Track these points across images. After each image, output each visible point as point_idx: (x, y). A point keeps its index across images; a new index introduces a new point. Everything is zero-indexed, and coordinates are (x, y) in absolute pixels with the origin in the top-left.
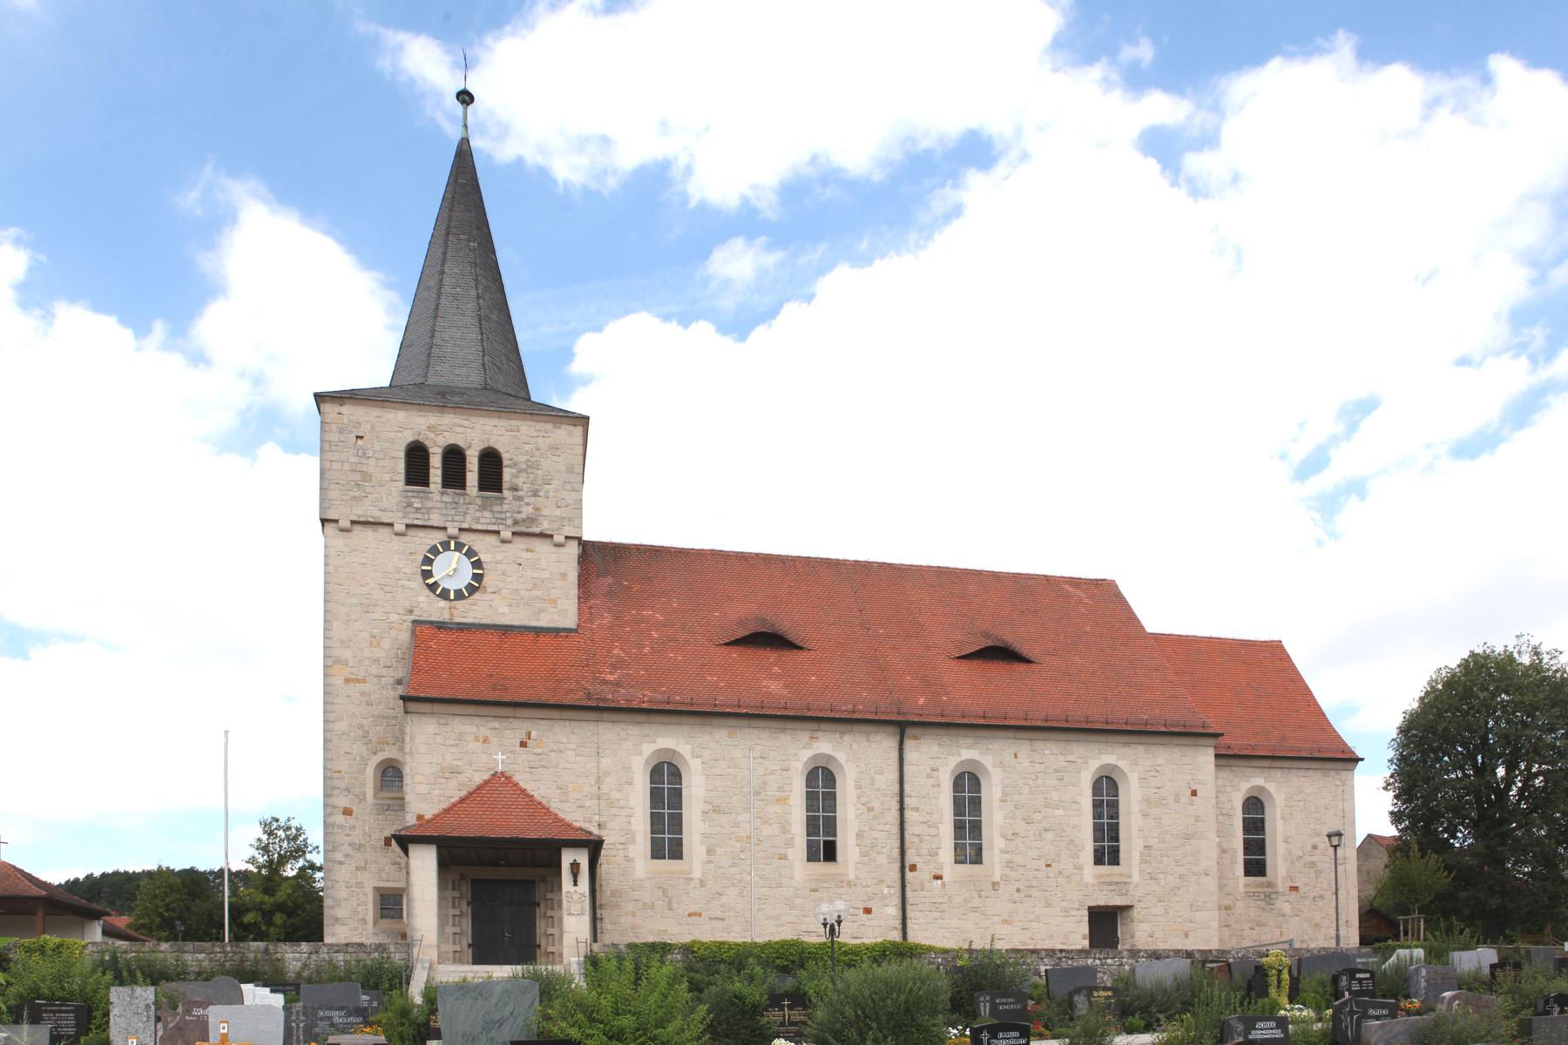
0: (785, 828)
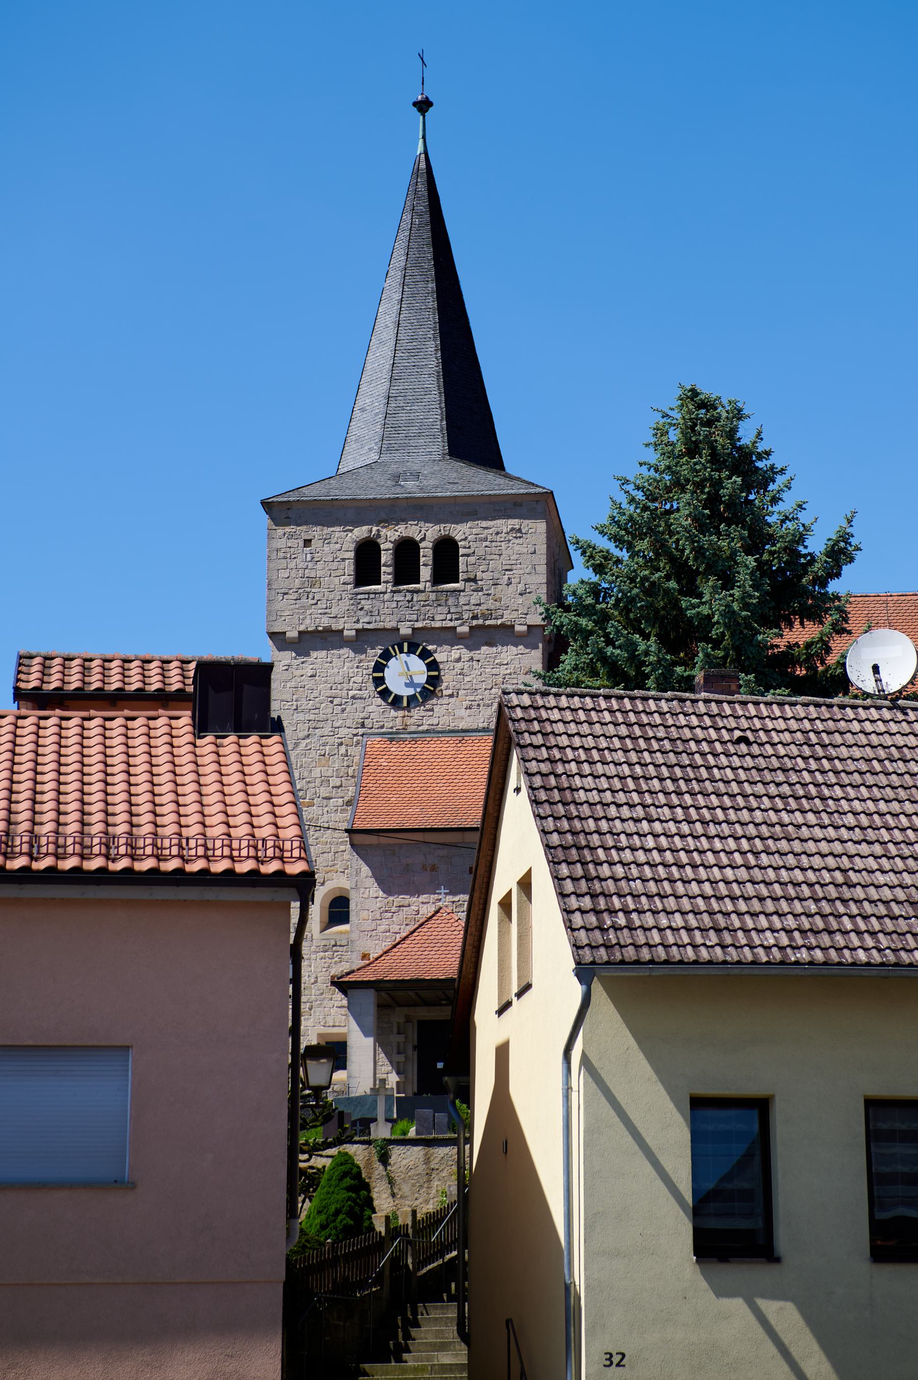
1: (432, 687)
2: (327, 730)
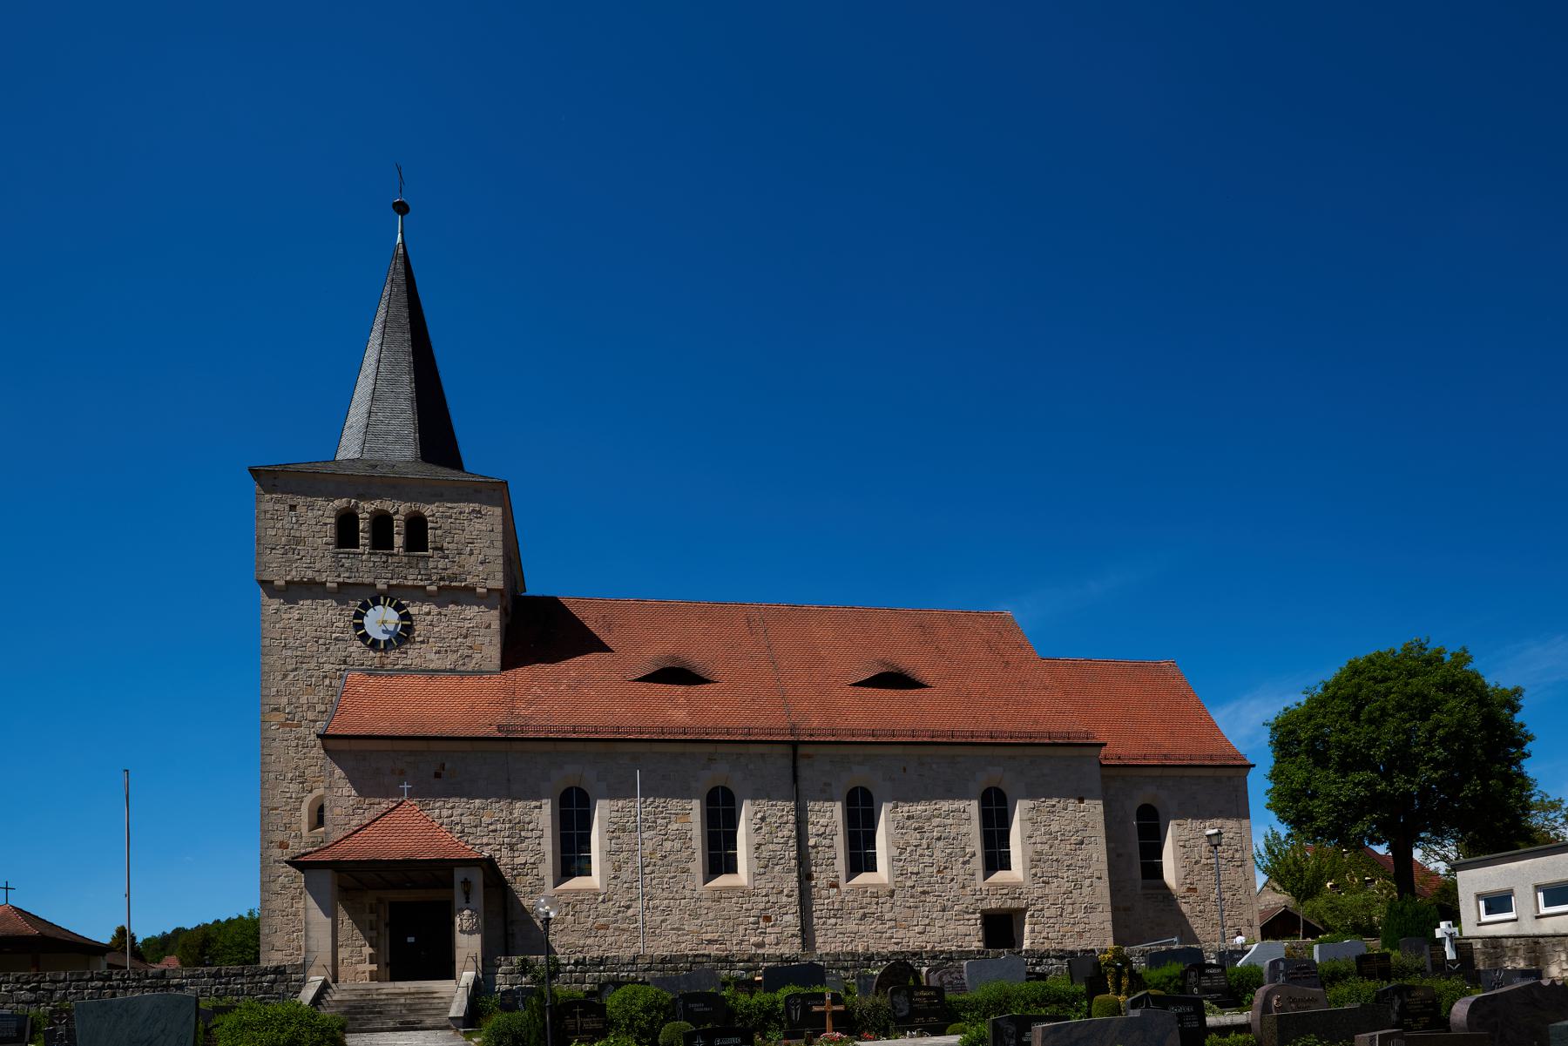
1: (404, 635)
2: (313, 665)
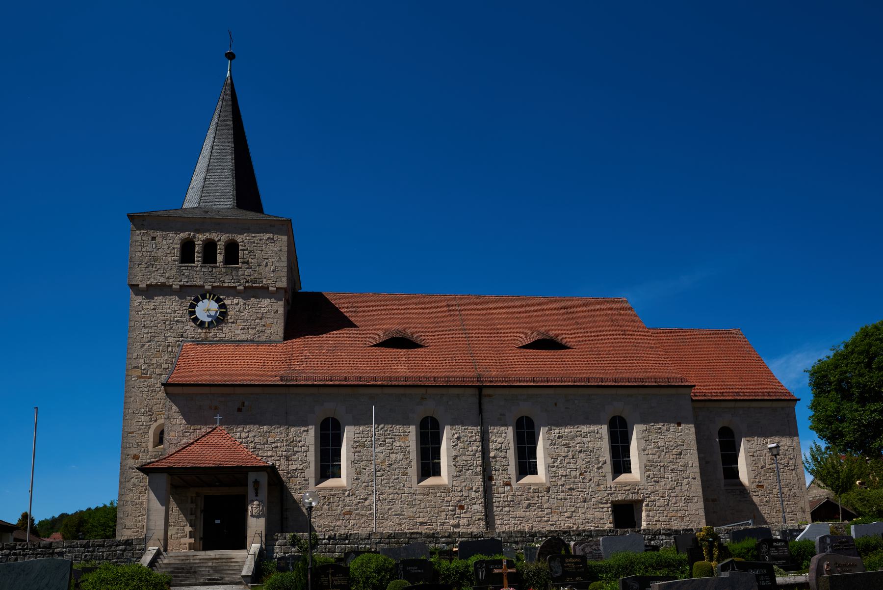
0: (404, 451)
2: (161, 338)
